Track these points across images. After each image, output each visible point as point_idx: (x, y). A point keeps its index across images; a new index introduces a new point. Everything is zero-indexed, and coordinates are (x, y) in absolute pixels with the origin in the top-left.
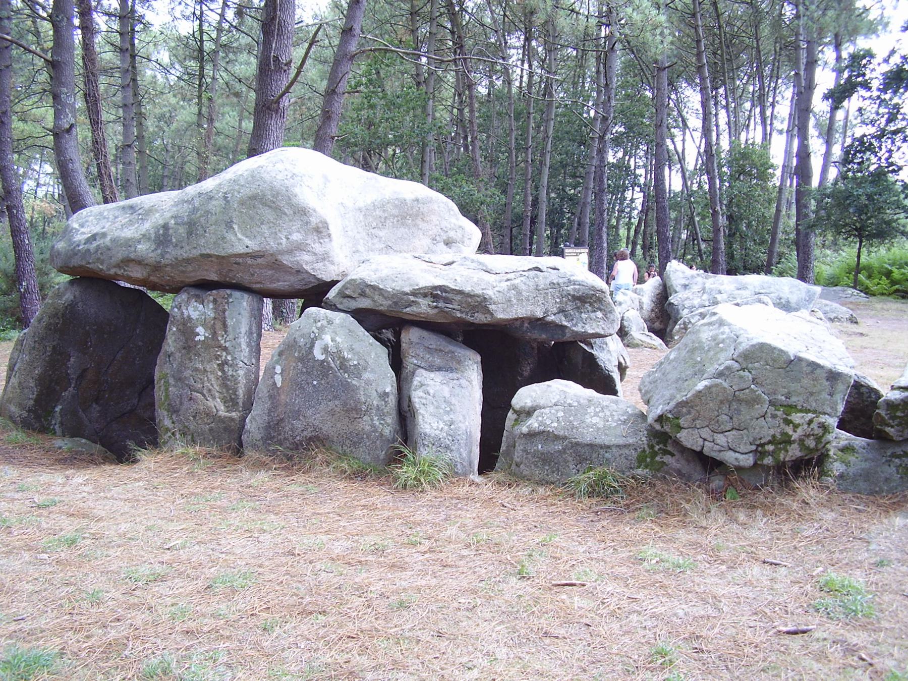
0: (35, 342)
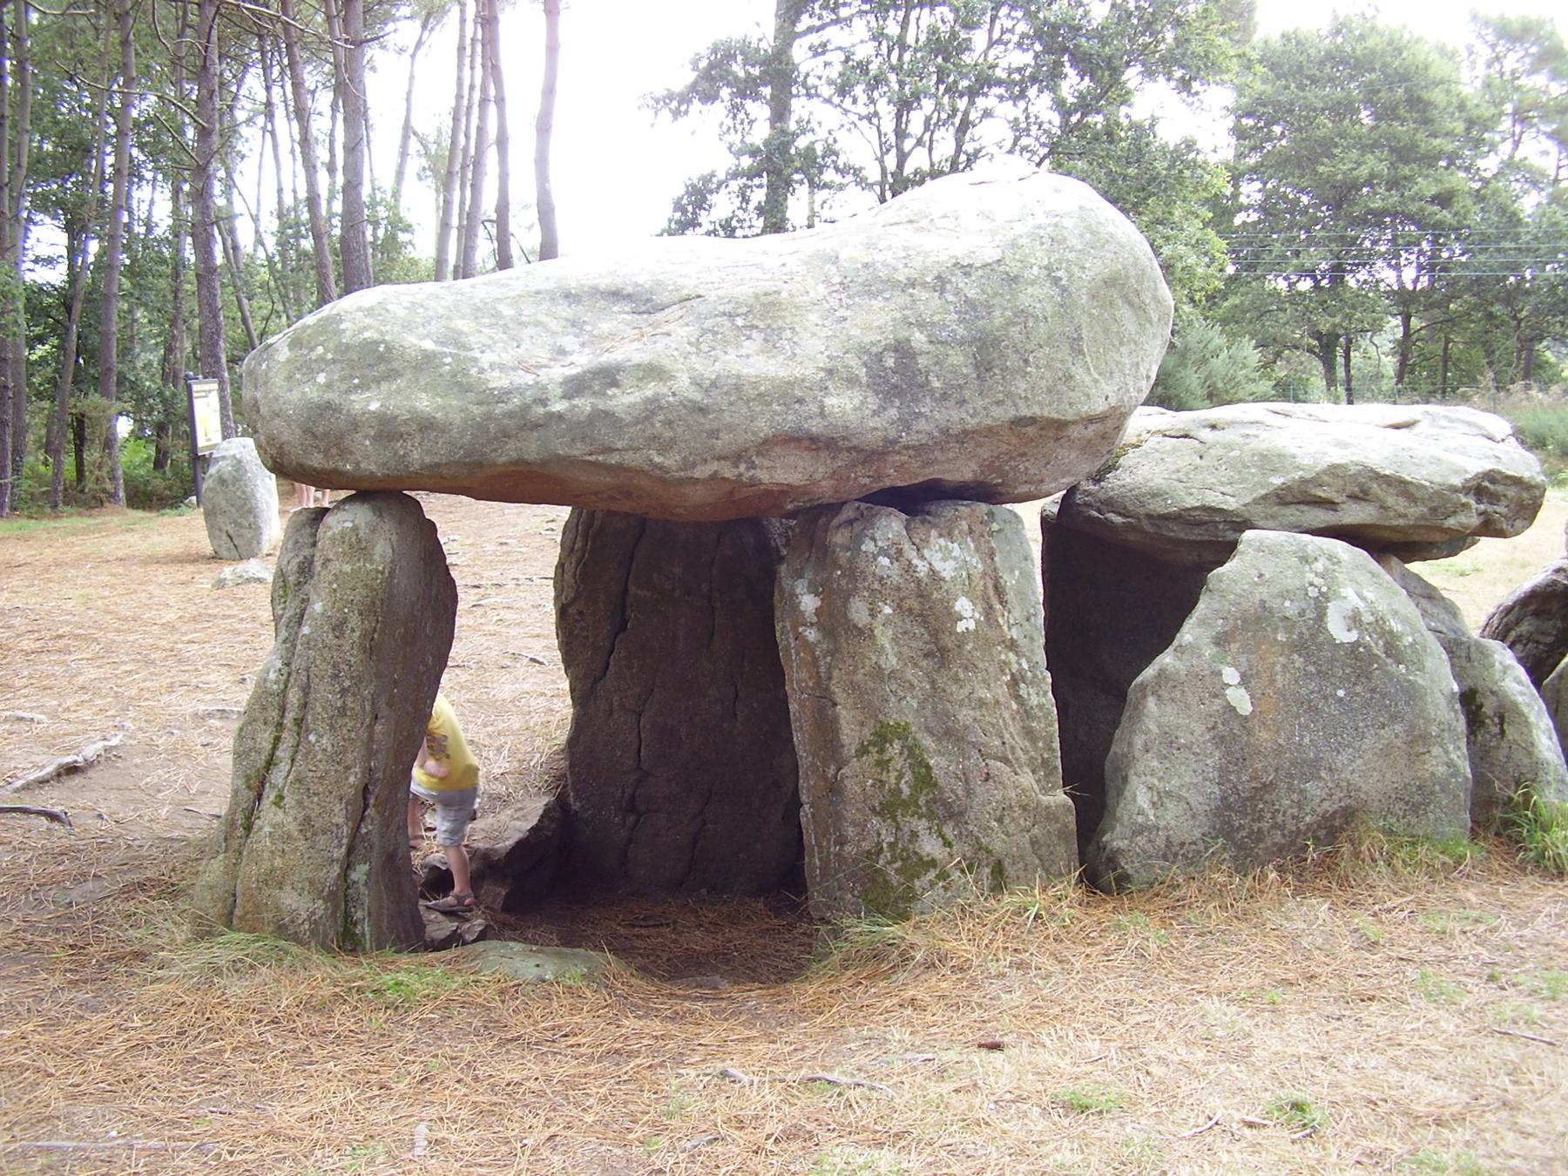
0: (344, 691)
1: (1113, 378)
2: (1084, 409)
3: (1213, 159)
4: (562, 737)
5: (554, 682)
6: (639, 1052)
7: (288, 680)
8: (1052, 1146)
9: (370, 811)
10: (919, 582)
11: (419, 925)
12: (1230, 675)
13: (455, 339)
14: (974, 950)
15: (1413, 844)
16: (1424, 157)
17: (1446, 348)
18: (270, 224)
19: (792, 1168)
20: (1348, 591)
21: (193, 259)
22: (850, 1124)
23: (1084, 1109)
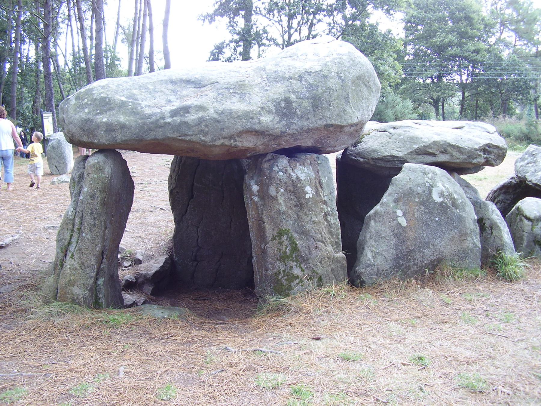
0: (95, 219)
1: (360, 110)
2: (350, 122)
3: (397, 38)
4: (171, 235)
5: (168, 216)
6: (197, 342)
7: (75, 215)
8: (337, 372)
9: (104, 260)
10: (293, 181)
11: (122, 300)
12: (399, 213)
13: (133, 97)
14: (312, 306)
15: (461, 270)
16: (469, 37)
17: (477, 103)
18: (70, 58)
19: (249, 380)
20: (440, 184)
21: (43, 70)
22: (269, 365)
23: (348, 359)
